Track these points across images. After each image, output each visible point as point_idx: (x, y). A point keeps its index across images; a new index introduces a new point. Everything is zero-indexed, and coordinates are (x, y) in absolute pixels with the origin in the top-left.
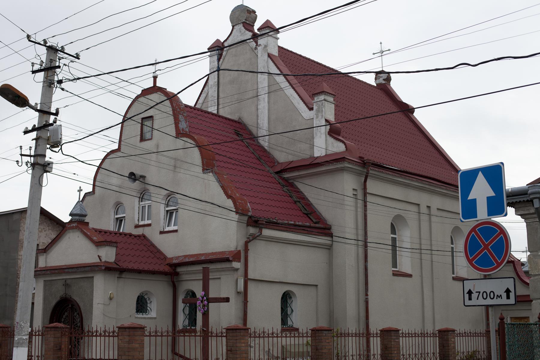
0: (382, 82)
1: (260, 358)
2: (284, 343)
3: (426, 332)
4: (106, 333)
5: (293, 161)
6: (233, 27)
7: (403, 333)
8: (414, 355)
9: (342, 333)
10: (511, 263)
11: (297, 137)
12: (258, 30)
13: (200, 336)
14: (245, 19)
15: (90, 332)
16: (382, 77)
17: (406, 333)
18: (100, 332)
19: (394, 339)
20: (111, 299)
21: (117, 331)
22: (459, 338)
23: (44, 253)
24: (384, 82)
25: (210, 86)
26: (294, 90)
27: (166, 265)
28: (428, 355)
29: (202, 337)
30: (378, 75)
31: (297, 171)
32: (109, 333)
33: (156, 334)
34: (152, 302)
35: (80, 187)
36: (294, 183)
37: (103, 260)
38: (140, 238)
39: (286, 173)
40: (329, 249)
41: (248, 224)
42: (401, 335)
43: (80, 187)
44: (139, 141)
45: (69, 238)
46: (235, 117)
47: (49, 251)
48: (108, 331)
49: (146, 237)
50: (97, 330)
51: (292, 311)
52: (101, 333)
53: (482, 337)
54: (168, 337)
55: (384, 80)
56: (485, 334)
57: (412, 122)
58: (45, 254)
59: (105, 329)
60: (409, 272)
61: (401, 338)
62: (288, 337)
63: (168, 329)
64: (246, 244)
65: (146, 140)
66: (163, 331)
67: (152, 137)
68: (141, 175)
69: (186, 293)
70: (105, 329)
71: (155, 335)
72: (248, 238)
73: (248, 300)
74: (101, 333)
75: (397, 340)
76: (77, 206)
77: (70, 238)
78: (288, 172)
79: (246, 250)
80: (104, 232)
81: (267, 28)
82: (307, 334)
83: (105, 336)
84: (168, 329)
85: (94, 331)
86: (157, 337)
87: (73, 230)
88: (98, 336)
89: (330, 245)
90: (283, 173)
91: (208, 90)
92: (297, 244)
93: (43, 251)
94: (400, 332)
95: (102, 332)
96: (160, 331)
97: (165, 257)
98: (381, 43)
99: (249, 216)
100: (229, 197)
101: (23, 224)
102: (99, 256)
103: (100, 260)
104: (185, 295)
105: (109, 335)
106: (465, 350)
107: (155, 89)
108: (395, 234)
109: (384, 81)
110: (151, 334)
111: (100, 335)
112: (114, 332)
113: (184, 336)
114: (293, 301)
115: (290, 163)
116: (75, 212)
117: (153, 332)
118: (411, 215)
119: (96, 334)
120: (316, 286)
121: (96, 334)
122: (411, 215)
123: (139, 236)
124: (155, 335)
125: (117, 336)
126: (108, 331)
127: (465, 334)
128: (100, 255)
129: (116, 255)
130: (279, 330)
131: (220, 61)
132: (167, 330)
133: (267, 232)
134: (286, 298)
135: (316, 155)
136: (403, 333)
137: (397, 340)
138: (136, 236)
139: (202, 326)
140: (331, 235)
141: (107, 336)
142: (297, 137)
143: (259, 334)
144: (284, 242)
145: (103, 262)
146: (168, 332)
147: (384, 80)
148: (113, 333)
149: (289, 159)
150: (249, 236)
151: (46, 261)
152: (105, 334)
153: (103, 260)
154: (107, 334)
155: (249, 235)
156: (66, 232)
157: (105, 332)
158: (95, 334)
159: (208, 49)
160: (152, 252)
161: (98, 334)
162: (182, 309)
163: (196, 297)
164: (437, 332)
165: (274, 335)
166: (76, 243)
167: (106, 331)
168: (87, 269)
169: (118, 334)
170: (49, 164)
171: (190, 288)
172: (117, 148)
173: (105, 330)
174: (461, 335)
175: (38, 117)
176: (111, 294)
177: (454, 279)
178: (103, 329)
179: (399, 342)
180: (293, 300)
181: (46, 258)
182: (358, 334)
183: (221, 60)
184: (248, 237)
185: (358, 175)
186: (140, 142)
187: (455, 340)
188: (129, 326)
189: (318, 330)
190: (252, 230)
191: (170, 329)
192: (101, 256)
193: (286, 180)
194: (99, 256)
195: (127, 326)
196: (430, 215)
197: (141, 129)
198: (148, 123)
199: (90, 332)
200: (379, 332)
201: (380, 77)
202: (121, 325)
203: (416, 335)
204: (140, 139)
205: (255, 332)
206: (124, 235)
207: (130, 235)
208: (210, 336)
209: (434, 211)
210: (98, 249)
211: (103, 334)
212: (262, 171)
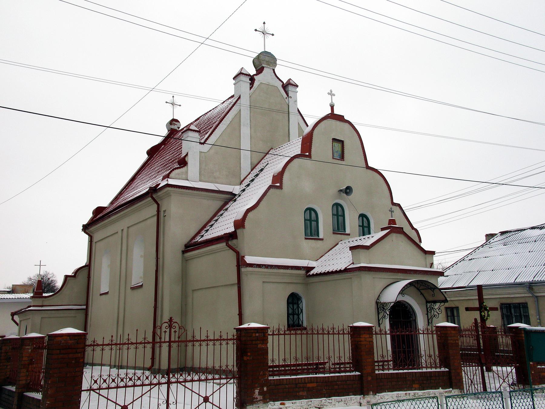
13: (348, 334)
29: (350, 335)
33: (279, 333)
53: (430, 336)
56: (435, 332)
62: (341, 334)
66: (339, 330)
71: (289, 333)
82: (343, 331)
92: (217, 252)
95: (330, 329)
96: (316, 329)
98: (264, 23)
124: (322, 333)
189: (529, 323)
201: (175, 124)
205: (427, 328)
212: (5, 298)
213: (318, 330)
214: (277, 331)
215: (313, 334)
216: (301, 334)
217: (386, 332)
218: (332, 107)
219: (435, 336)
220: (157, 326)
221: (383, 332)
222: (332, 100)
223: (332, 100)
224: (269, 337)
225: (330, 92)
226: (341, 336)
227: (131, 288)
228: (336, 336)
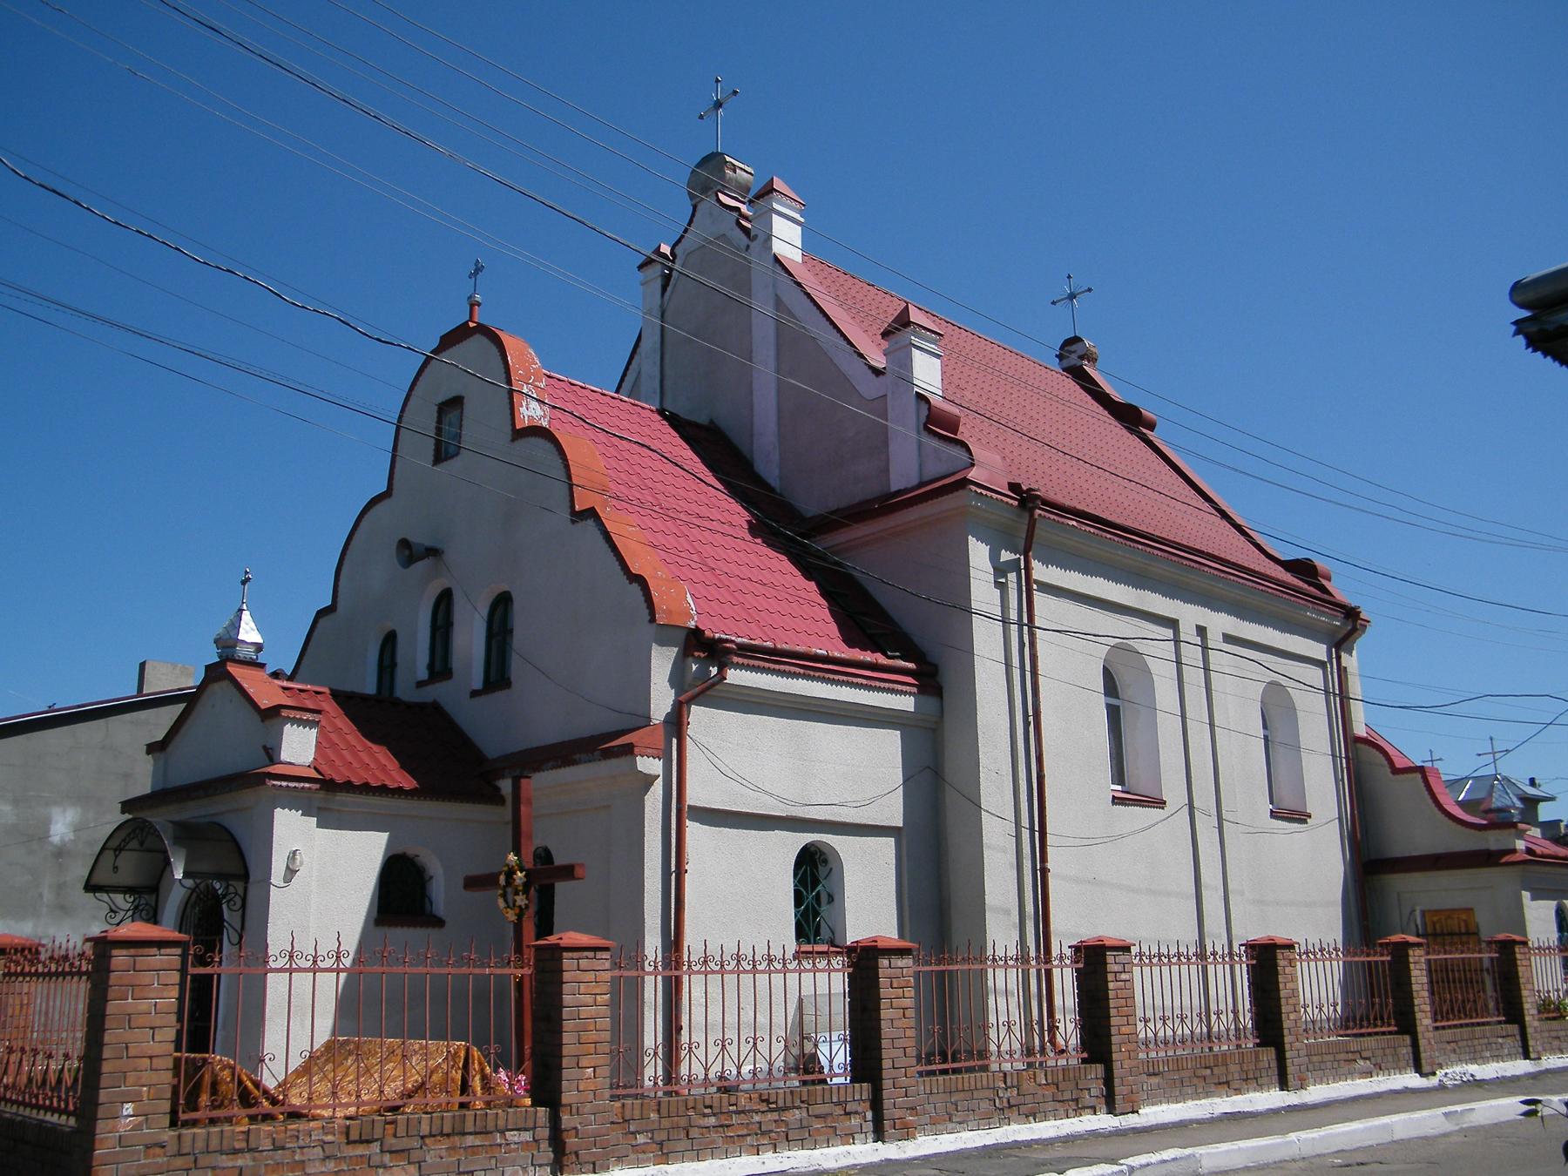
1: (726, 1038)
2: (808, 990)
7: (1141, 954)
8: (1178, 1017)
9: (997, 957)
10: (1415, 772)
16: (1075, 352)
17: (1152, 953)
19: (1116, 973)
22: (1320, 964)
28: (1219, 1018)
42: (1138, 958)
46: (702, 419)
61: (1137, 970)
71: (288, 966)
75: (1124, 976)
91: (639, 365)
94: (1134, 950)
106: (1324, 1001)
108: (1117, 697)
113: (815, 970)
117: (1012, 958)
118: (1156, 649)
122: (1156, 649)
127: (1323, 954)
128: (268, 746)
130: (790, 954)
136: (1141, 954)
137: (1124, 976)
139: (660, 949)
146: (770, 961)
163: (553, 863)
164: (1243, 948)
165: (712, 965)
170: (1364, 1020)
174: (1312, 957)
175: (901, 790)
177: (1273, 815)
179: (1131, 981)
182: (1001, 959)
183: (669, 289)
187: (1489, 1015)
196: (1205, 648)
200: (1068, 952)
203: (1182, 958)
209: (1214, 639)
213: (722, 962)
224: (647, 978)
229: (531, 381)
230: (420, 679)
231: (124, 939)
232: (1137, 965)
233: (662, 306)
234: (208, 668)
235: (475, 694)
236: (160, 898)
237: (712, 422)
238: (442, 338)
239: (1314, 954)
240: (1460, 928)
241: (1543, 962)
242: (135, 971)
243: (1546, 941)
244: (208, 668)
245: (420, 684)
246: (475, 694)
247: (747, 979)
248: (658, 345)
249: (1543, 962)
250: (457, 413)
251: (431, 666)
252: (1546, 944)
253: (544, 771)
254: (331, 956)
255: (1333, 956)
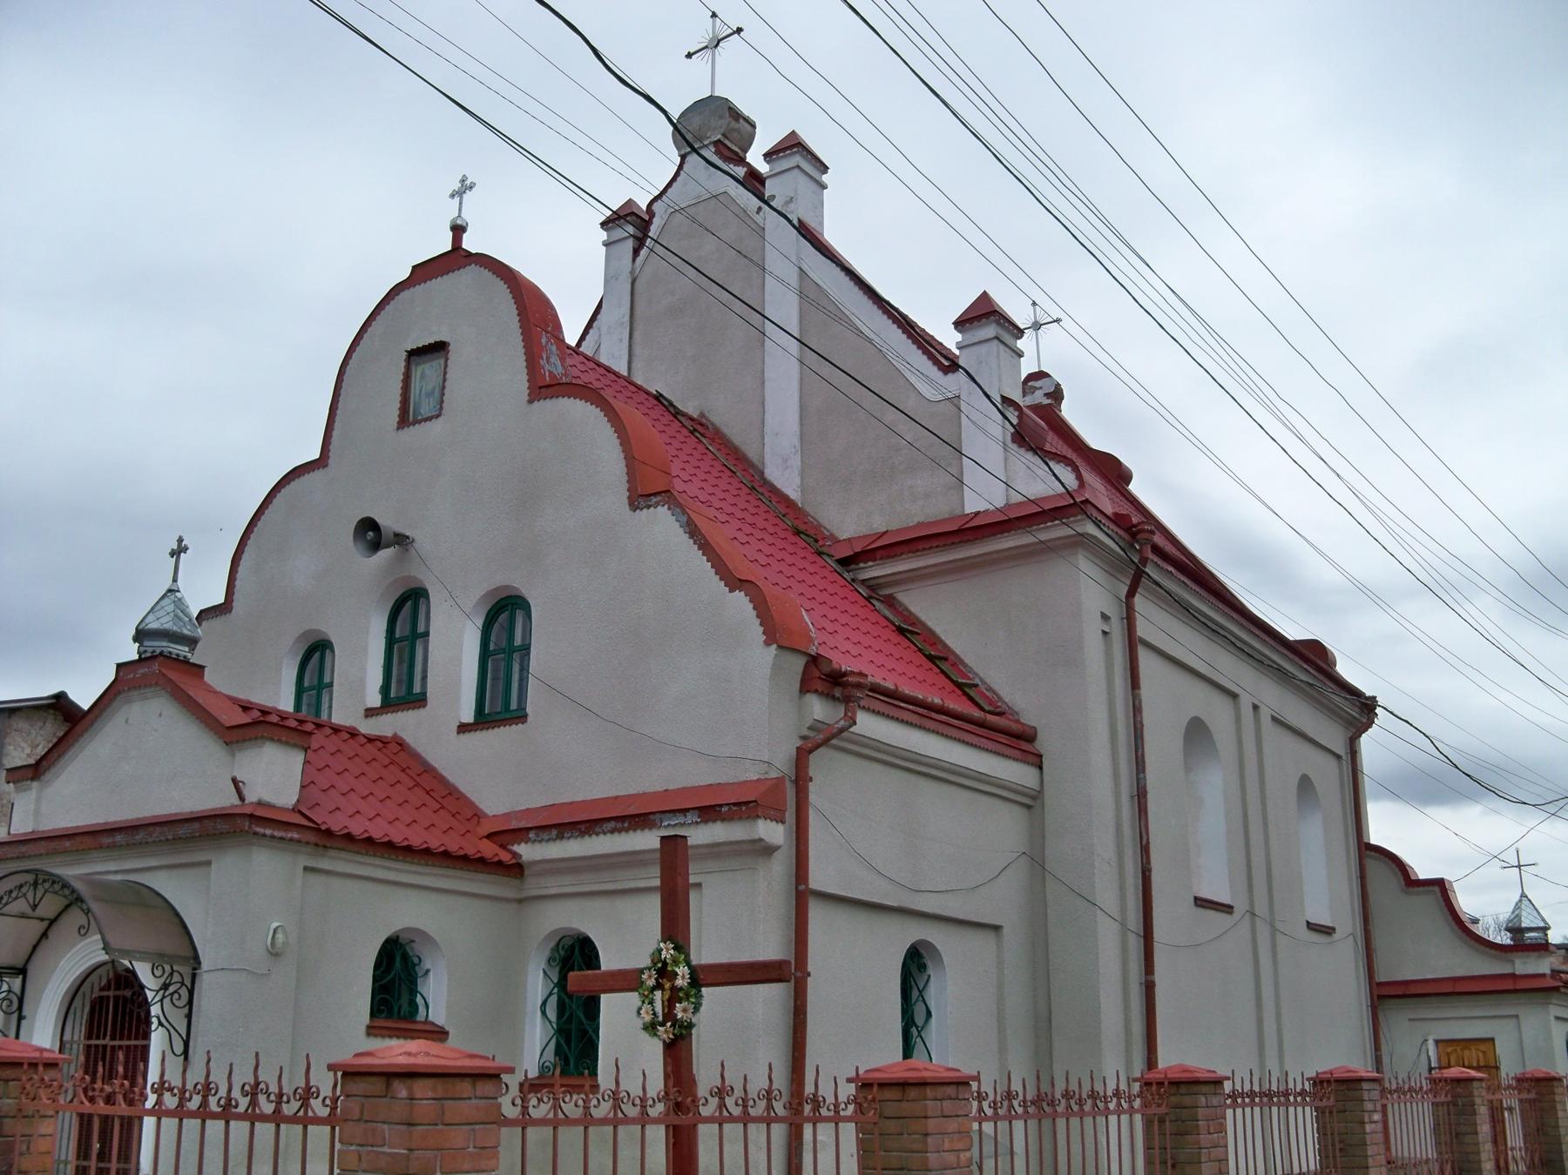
0: (1040, 401)
3: (1060, 1087)
4: (262, 1098)
5: (887, 531)
6: (683, 157)
11: (899, 458)
12: (769, 156)
14: (722, 131)
15: (171, 1089)
16: (1041, 388)
18: (223, 1092)
20: (274, 953)
21: (326, 1091)
23: (33, 779)
24: (1047, 401)
25: (604, 330)
26: (889, 318)
27: (485, 840)
30: (1030, 384)
31: (910, 555)
32: (279, 1103)
33: (556, 1114)
34: (431, 974)
35: (180, 540)
36: (894, 598)
37: (251, 797)
38: (385, 747)
39: (870, 563)
40: (1029, 807)
41: (805, 687)
43: (180, 540)
44: (396, 425)
45: (127, 721)
47: (48, 776)
48: (274, 1088)
49: (408, 745)
50: (211, 1079)
51: (929, 1014)
52: (229, 1099)
54: (615, 1127)
55: (1047, 395)
57: (1131, 503)
58: (35, 784)
59: (256, 1077)
60: (1224, 898)
63: (617, 1083)
64: (802, 757)
65: (419, 422)
67: (441, 408)
68: (397, 532)
69: (553, 944)
70: (256, 1077)
71: (551, 1115)
72: (803, 738)
73: (809, 970)
74: (229, 1099)
76: (163, 603)
77: (130, 721)
78: (881, 559)
79: (801, 780)
80: (260, 711)
81: (795, 150)
83: (253, 1117)
84: (617, 1083)
85: (189, 1086)
86: (560, 1129)
87: (142, 691)
88: (215, 1116)
89: (1034, 793)
90: (862, 565)
93: (30, 773)
94: (1227, 1086)
95: (236, 1093)
97: (477, 815)
99: (810, 655)
100: (734, 582)
101: (12, 748)
102: (235, 781)
103: (242, 798)
104: (552, 950)
105: (277, 1111)
107: (456, 258)
109: (1048, 398)
110: (531, 1110)
111: (227, 1112)
112: (307, 1094)
114: (932, 978)
115: (878, 535)
116: (154, 625)
119: (205, 1103)
120: (997, 928)
121: (205, 1103)
123: (383, 742)
125: (330, 1121)
126: (274, 1088)
129: (303, 787)
131: (639, 255)
132: (641, 1094)
133: (869, 725)
134: (916, 963)
135: (970, 509)
138: (373, 738)
140: (1037, 761)
141: (264, 1118)
142: (899, 458)
143: (995, 1103)
144: (912, 766)
145: (252, 803)
147: (1047, 395)
148: (305, 1104)
149: (875, 526)
150: (809, 728)
151: (37, 812)
152: (254, 1103)
153: (251, 797)
154: (267, 1108)
155: (810, 728)
156: (119, 698)
157: (253, 1091)
158: (194, 1104)
159: (601, 224)
160: (431, 793)
161: (213, 1101)
162: (540, 1003)
166: (150, 738)
167: (262, 1086)
168: (182, 831)
169: (334, 1109)
171: (574, 926)
172: (316, 455)
173: (257, 1084)
176: (280, 930)
178: (243, 1076)
180: (929, 976)
181: (38, 801)
184: (805, 732)
185: (1111, 572)
186: (398, 429)
188: (412, 1060)
190: (819, 709)
191: (781, 1082)
192: (242, 782)
193: (873, 586)
194: (235, 781)
195: (1178, 1075)
197: (402, 388)
198: (427, 371)
199: (171, 1089)
201: (1036, 388)
202: (357, 1055)
204: (397, 419)
206: (330, 731)
207: (353, 733)
208: (808, 1120)
209: (1265, 715)
210: (233, 755)
211: (244, 1103)
213: (836, 1105)
214: (762, 1104)
215: (615, 1123)
216: (555, 1124)
217: (229, 1104)
218: (458, 230)
219: (1138, 1118)
220: (185, 1006)
221: (824, 1112)
222: (460, 210)
223: (460, 210)
224: (703, 1129)
225: (468, 182)
226: (239, 1129)
227: (1196, 899)
228: (215, 1127)
229: (550, 329)
230: (369, 706)
231: (1146, 1045)
232: (1229, 1107)
233: (632, 272)
234: (120, 667)
235: (463, 728)
236: (1362, 972)
237: (702, 415)
238: (414, 268)
239: (1080, 1103)
240: (1478, 1060)
241: (1409, 1110)
242: (443, 1124)
243: (1406, 1080)
244: (120, 667)
245: (370, 713)
246: (463, 728)
247: (629, 1133)
248: (627, 318)
249: (1409, 1110)
250: (442, 361)
251: (385, 689)
252: (1247, 1088)
253: (597, 834)
254: (761, 1097)
255: (1112, 1106)
